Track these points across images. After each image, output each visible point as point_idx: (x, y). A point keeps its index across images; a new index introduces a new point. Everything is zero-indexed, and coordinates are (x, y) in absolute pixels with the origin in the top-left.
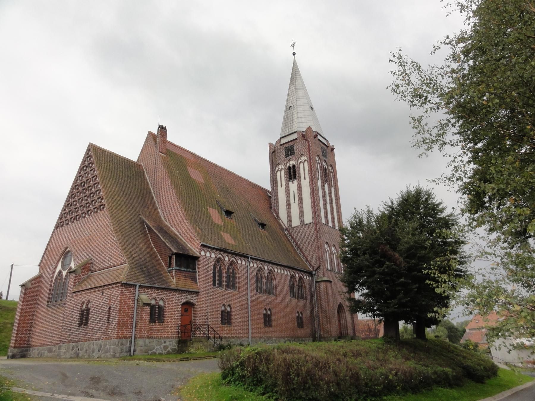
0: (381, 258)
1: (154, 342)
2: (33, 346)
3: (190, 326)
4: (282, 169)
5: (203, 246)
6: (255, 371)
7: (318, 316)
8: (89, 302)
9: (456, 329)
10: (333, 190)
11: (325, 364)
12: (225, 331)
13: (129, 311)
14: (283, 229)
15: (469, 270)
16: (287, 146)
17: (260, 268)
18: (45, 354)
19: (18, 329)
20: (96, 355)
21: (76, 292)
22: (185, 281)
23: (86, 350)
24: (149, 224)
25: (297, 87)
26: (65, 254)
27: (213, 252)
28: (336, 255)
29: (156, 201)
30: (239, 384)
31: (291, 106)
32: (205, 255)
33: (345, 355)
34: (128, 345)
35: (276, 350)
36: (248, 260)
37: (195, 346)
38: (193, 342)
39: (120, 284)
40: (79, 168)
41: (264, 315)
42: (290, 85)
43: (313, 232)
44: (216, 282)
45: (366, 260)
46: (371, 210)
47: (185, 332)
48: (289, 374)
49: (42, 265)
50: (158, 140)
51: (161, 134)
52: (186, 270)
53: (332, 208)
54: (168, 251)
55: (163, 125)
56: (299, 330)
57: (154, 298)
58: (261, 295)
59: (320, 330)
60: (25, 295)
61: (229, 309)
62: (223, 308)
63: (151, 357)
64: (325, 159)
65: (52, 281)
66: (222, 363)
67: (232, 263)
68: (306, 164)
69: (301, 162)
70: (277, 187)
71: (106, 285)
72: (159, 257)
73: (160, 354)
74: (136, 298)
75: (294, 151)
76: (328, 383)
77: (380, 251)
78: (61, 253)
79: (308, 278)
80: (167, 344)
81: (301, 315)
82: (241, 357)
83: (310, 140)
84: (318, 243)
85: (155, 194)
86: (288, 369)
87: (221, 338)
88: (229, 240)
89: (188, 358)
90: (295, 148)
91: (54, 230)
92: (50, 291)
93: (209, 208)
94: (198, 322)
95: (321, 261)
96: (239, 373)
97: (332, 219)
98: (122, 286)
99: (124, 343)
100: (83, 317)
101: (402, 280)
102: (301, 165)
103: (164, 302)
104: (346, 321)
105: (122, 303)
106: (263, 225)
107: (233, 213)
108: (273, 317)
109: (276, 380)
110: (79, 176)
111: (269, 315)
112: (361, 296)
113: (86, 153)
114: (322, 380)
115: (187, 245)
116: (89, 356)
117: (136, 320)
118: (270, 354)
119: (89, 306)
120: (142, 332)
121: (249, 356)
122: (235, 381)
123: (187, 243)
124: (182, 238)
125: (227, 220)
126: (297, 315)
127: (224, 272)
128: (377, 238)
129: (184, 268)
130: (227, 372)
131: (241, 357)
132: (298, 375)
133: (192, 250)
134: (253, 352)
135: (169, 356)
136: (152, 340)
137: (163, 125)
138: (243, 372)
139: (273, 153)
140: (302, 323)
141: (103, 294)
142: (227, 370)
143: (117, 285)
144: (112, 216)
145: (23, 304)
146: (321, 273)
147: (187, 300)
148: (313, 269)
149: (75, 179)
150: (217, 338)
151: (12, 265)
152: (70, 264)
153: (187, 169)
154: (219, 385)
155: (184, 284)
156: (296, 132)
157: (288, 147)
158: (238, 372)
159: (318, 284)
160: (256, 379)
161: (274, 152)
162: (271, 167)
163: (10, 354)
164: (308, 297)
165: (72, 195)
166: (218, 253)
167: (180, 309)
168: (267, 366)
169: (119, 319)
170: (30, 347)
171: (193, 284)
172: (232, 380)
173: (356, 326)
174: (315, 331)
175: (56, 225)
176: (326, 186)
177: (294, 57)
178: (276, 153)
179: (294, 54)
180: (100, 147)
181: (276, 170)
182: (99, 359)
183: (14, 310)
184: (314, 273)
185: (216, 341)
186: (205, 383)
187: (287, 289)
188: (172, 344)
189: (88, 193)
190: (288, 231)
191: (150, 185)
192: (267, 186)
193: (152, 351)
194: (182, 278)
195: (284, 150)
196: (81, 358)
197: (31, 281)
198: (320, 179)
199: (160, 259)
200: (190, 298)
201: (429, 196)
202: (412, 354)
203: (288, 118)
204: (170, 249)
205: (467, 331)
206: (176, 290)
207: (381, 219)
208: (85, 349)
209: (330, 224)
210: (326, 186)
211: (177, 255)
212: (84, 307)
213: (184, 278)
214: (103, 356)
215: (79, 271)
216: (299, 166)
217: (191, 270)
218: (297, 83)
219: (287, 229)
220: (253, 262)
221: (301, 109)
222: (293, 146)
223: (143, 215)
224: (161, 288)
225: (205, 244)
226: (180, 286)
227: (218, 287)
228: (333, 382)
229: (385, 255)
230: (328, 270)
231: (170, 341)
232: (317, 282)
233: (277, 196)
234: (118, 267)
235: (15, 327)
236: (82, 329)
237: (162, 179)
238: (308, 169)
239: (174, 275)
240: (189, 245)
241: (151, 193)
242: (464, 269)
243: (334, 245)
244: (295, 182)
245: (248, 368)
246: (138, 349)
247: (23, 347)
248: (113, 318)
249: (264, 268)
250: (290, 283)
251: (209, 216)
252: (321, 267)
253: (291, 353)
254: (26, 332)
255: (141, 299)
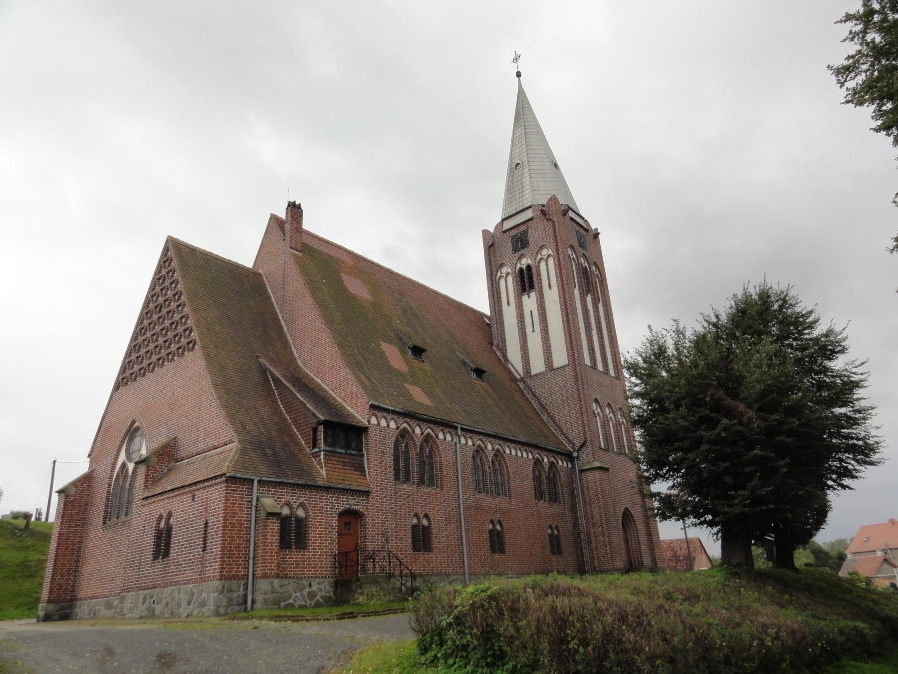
0: (711, 412)
1: (291, 586)
2: (81, 599)
3: (355, 554)
4: (508, 274)
5: (373, 407)
6: (488, 635)
7: (588, 534)
8: (170, 515)
9: (826, 554)
10: (600, 306)
11: (638, 617)
12: (420, 564)
13: (240, 527)
14: (515, 380)
15: (872, 434)
16: (514, 232)
17: (479, 446)
18: (101, 613)
19: (54, 569)
20: (184, 611)
21: (149, 497)
22: (343, 471)
23: (167, 604)
24: (275, 372)
25: (527, 131)
26: (132, 433)
27: (393, 419)
28: (612, 422)
29: (287, 333)
30: (455, 663)
31: (518, 164)
32: (379, 424)
33: (668, 597)
34: (241, 592)
35: (529, 590)
36: (456, 433)
37: (366, 591)
38: (362, 583)
39: (224, 478)
40: (152, 282)
41: (491, 532)
42: (514, 127)
43: (571, 381)
44: (401, 474)
45: (683, 418)
46: (681, 327)
47: (346, 566)
48: (564, 641)
49: (93, 455)
50: (288, 227)
51: (292, 217)
52: (344, 451)
53: (601, 338)
54: (300, 403)
55: (295, 202)
56: (554, 558)
57: (288, 504)
58: (481, 496)
59: (593, 558)
60: (65, 508)
61: (425, 522)
62: (415, 521)
63: (282, 613)
64: (583, 251)
65: (110, 481)
66: (417, 620)
67: (427, 439)
68: (551, 261)
69: (541, 259)
70: (501, 306)
71: (200, 482)
72: (295, 430)
73: (302, 607)
74: (254, 503)
75: (527, 240)
76: (651, 659)
77: (708, 398)
78: (124, 430)
79: (565, 465)
80: (315, 588)
81: (556, 532)
82: (457, 607)
83: (555, 219)
84: (580, 400)
85: (285, 321)
86: (562, 628)
87: (413, 576)
88: (419, 397)
89: (352, 613)
90: (530, 235)
91: (113, 392)
92: (108, 499)
93: (382, 343)
94: (370, 546)
95: (588, 432)
96: (454, 641)
97: (602, 358)
98: (226, 481)
99: (234, 587)
100: (161, 542)
101: (757, 452)
102: (543, 265)
103: (306, 511)
104: (638, 540)
105: (229, 513)
106: (479, 372)
107: (425, 351)
108: (507, 537)
109: (536, 655)
110: (152, 296)
111: (498, 532)
112: (673, 487)
113: (162, 255)
114: (639, 651)
115: (344, 407)
116: (172, 613)
117: (255, 544)
118: (519, 597)
119: (171, 521)
120: (267, 566)
121: (474, 603)
122: (446, 657)
123: (344, 404)
124: (336, 396)
125: (415, 363)
126: (549, 531)
127: (413, 455)
128: (700, 376)
129: (342, 448)
130: (429, 639)
131: (457, 607)
132: (585, 643)
133: (353, 417)
134: (483, 594)
135: (317, 610)
136: (285, 582)
137: (295, 202)
138: (461, 638)
139: (491, 246)
140: (559, 545)
141: (193, 499)
142: (429, 635)
143: (218, 480)
144: (209, 359)
145: (62, 525)
146: (588, 455)
147: (348, 506)
148: (574, 448)
149: (146, 300)
150: (406, 576)
151: (54, 462)
152: (140, 450)
153: (341, 277)
154: (413, 666)
155: (342, 478)
156: (530, 207)
157: (517, 235)
158: (451, 638)
159: (583, 475)
160: (489, 653)
161: (492, 245)
162: (489, 271)
163: (41, 613)
164: (567, 499)
165: (141, 329)
166: (401, 420)
167: (335, 523)
168: (515, 623)
169: (222, 544)
170: (77, 600)
171: (358, 477)
172: (439, 655)
173: (657, 550)
174: (583, 560)
175: (116, 383)
176: (589, 299)
177: (519, 80)
178: (496, 246)
179: (519, 75)
180: (186, 244)
181: (498, 277)
182: (189, 619)
183: (46, 537)
184: (575, 454)
185: (404, 581)
186: (384, 663)
187: (530, 485)
188: (323, 588)
189: (167, 323)
190: (525, 383)
191: (276, 307)
192: (483, 305)
193: (286, 602)
194: (338, 466)
195: (510, 240)
196: (159, 617)
197: (74, 484)
198: (577, 287)
199: (297, 433)
200: (353, 502)
201: (784, 302)
202: (786, 597)
203: (513, 187)
204: (314, 414)
205: (849, 556)
206: (327, 489)
207: (700, 342)
208: (164, 602)
209: (600, 367)
210: (589, 299)
211: (327, 424)
212: (162, 524)
213: (341, 467)
214: (196, 612)
215: (154, 460)
216: (538, 268)
217: (353, 452)
218: (526, 124)
219: (522, 379)
220: (464, 436)
221: (536, 167)
222: (525, 233)
223: (265, 358)
224: (300, 485)
225: (377, 404)
226: (334, 481)
227: (404, 482)
228: (661, 656)
229: (717, 407)
230: (600, 448)
231: (319, 584)
232: (581, 471)
233: (501, 323)
234: (221, 448)
235: (50, 566)
236: (160, 564)
237: (296, 294)
238: (556, 270)
239: (322, 461)
240: (348, 408)
241: (278, 320)
242: (863, 434)
243: (609, 404)
244: (533, 294)
245: (471, 628)
246: (260, 598)
247: (65, 601)
248: (212, 542)
249: (486, 448)
250: (534, 472)
251: (382, 356)
252: (588, 444)
253: (564, 594)
254: (69, 574)
255: (263, 506)
